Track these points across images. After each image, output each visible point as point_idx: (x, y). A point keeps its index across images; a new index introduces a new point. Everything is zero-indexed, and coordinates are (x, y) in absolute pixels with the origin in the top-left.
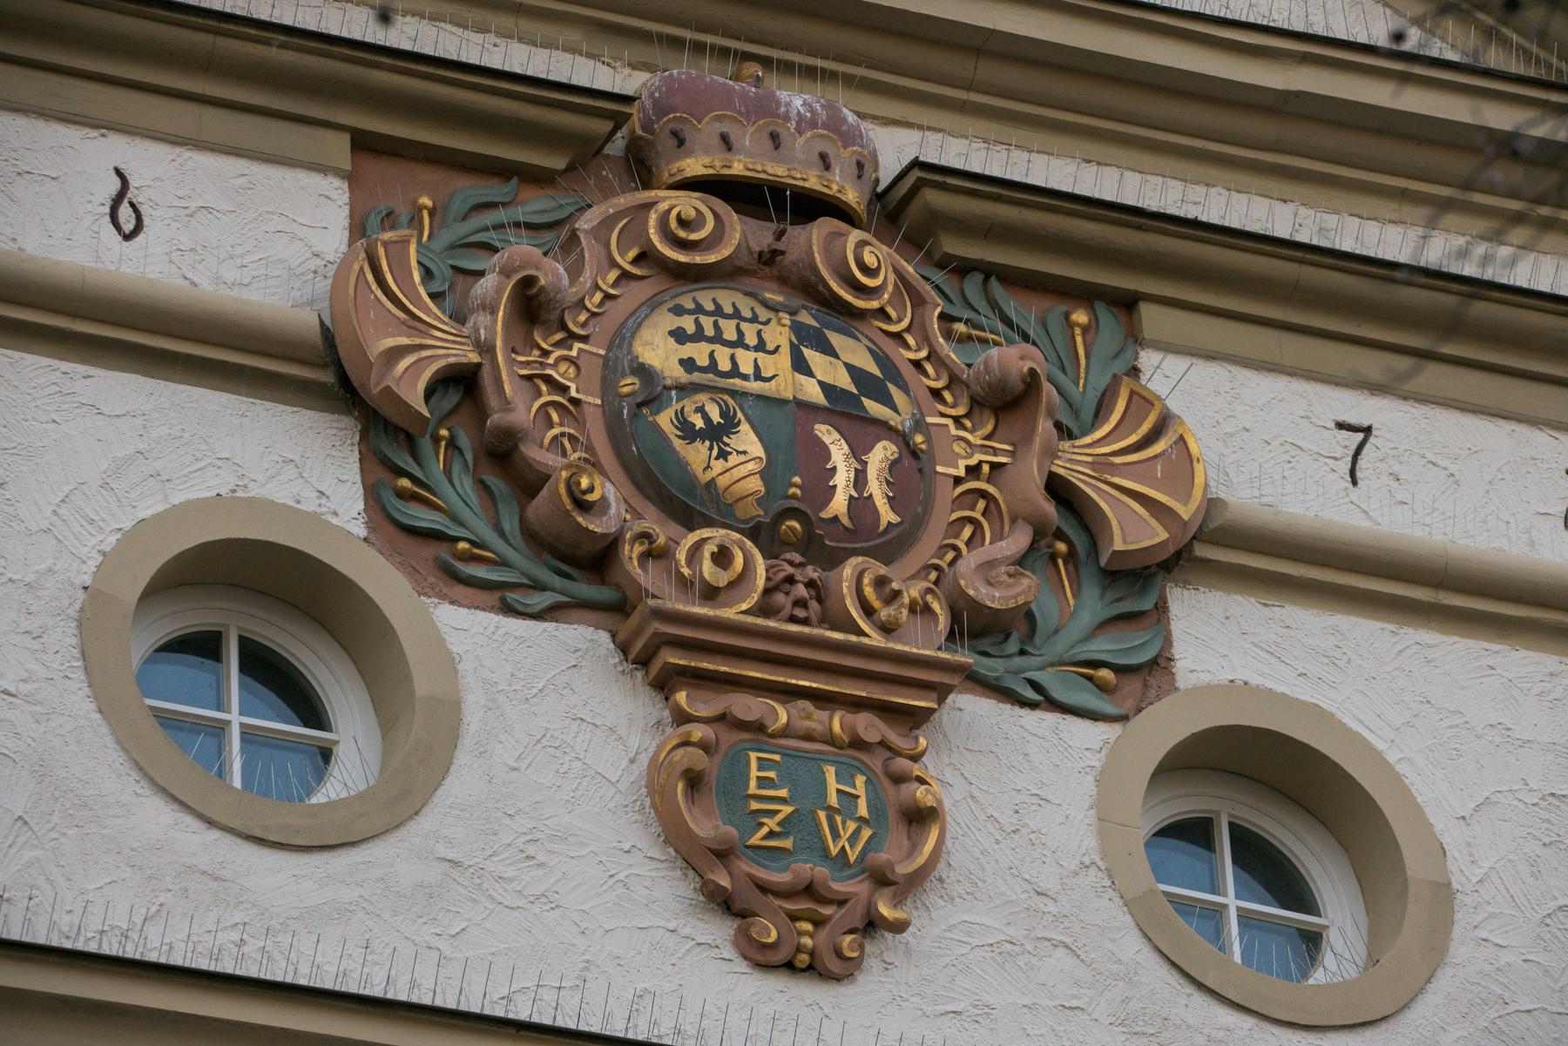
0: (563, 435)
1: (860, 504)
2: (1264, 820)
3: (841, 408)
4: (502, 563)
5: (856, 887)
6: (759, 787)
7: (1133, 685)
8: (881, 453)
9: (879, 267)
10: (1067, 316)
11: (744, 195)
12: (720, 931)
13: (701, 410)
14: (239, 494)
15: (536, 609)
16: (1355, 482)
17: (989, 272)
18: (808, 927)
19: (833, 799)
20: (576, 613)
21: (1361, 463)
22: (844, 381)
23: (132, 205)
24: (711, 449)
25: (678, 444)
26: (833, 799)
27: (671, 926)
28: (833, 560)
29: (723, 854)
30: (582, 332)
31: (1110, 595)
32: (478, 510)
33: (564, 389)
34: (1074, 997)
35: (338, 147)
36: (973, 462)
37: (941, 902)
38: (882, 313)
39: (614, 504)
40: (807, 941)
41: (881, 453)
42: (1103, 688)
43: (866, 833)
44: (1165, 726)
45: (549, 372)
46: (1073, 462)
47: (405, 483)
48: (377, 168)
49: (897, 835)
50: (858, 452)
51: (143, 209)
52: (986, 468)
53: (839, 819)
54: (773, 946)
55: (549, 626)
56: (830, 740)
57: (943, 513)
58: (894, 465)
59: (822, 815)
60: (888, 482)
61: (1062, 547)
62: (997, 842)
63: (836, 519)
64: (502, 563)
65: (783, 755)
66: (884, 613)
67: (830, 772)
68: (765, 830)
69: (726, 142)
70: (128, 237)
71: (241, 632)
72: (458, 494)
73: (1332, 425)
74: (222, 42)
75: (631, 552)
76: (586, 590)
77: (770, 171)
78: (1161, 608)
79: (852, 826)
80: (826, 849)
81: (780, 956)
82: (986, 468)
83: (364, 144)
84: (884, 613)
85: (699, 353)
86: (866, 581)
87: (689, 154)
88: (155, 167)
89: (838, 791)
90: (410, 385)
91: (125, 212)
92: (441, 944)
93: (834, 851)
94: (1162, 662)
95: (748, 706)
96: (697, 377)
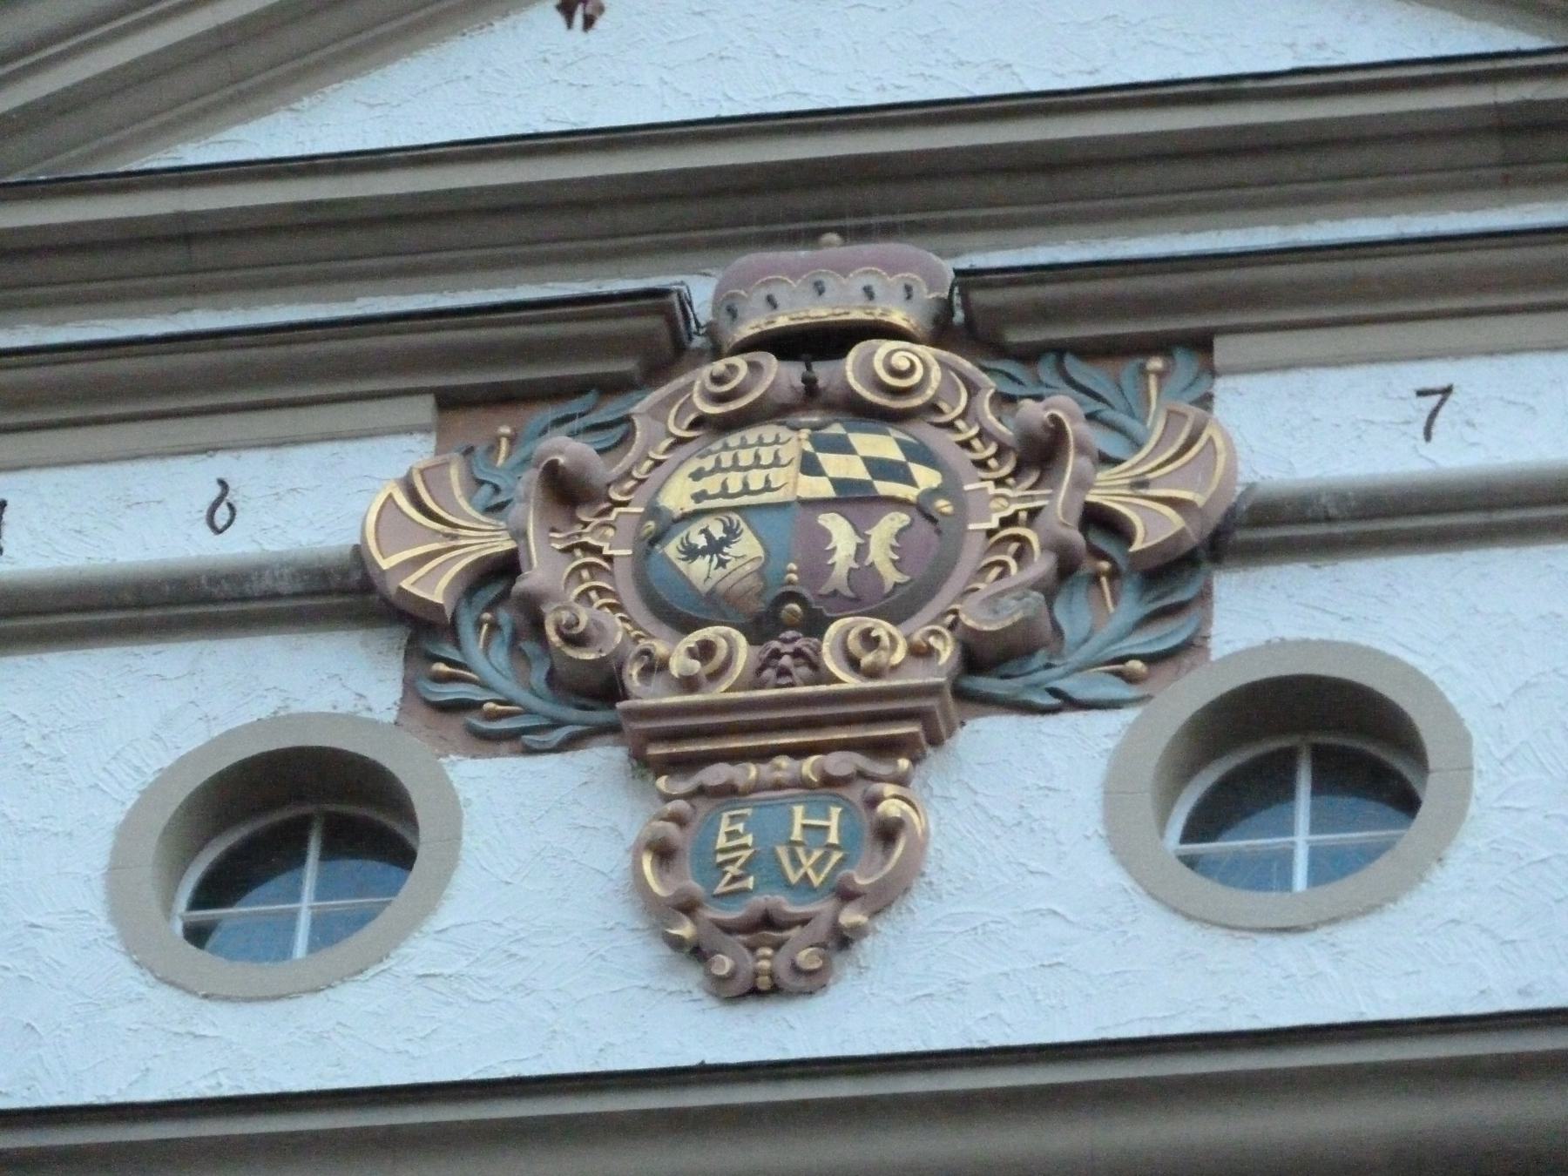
0: (591, 589)
1: (863, 571)
4: (528, 712)
5: (822, 907)
8: (891, 523)
9: (913, 365)
11: (786, 344)
12: (693, 976)
15: (554, 743)
16: (1428, 435)
18: (769, 952)
19: (797, 834)
21: (1439, 420)
22: (859, 472)
25: (681, 565)
26: (797, 834)
28: (815, 625)
29: (688, 907)
31: (1152, 594)
34: (1057, 955)
35: (424, 409)
42: (1131, 679)
43: (836, 856)
44: (1187, 695)
45: (585, 539)
46: (1108, 490)
47: (442, 667)
49: (869, 848)
52: (1023, 515)
54: (732, 975)
55: (568, 755)
57: (972, 554)
59: (783, 853)
61: (1105, 565)
63: (835, 593)
66: (867, 659)
68: (728, 876)
69: (771, 301)
70: (219, 532)
71: (288, 834)
72: (488, 662)
74: (298, 349)
75: (633, 672)
76: (600, 716)
78: (1205, 596)
83: (448, 402)
84: (867, 659)
87: (743, 321)
88: (249, 471)
90: (435, 587)
92: (410, 1048)
93: (794, 878)
94: (1197, 642)
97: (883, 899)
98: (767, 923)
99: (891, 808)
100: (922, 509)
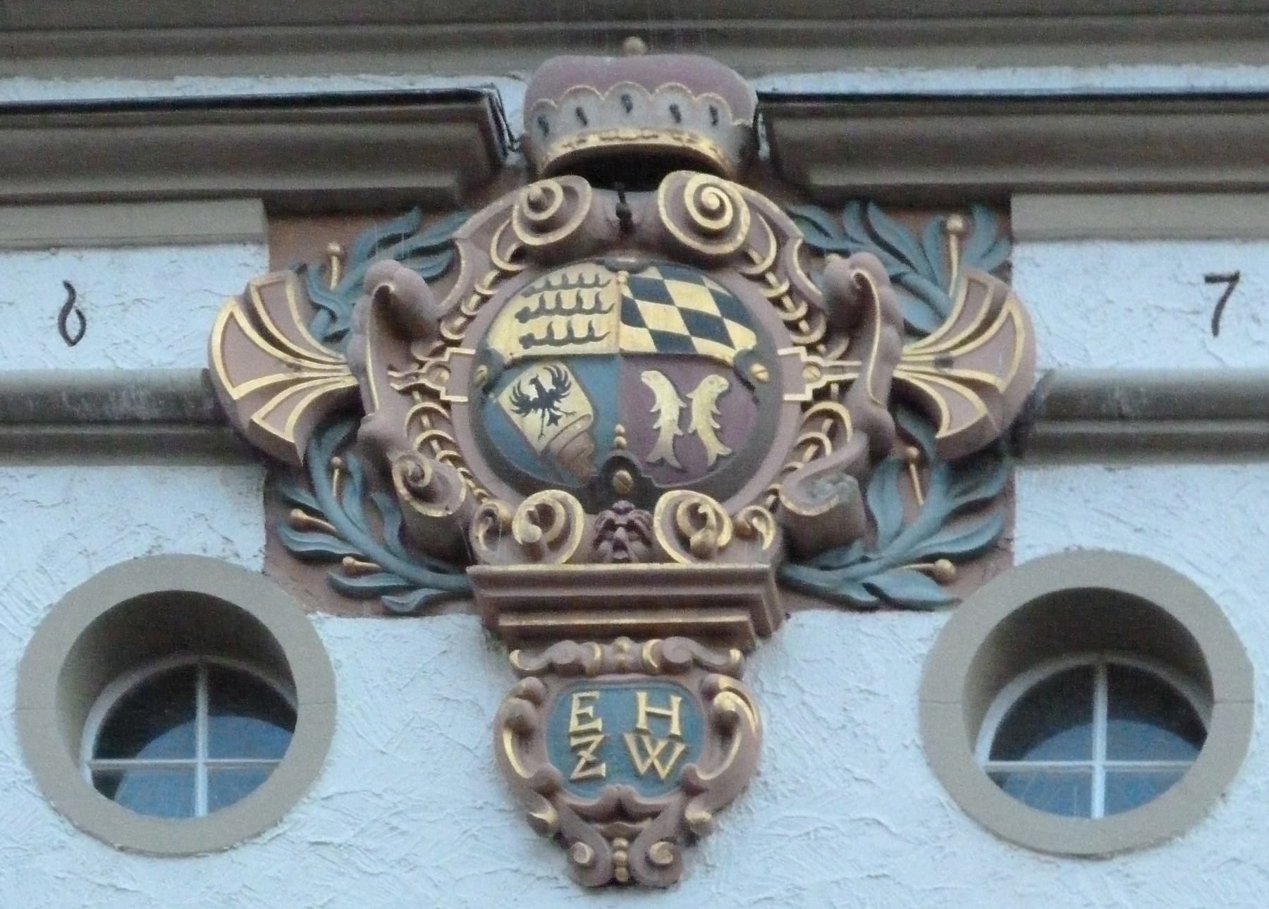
1: (687, 441)
2: (1101, 677)
3: (673, 355)
4: (385, 570)
5: (669, 800)
6: (580, 723)
7: (973, 572)
8: (711, 386)
10: (943, 225)
12: (556, 864)
13: (535, 381)
14: (156, 553)
17: (864, 198)
18: (624, 843)
19: (642, 723)
20: (452, 606)
21: (1226, 312)
22: (678, 326)
23: (79, 313)
24: (543, 416)
25: (515, 418)
26: (642, 723)
27: (513, 866)
28: (645, 496)
30: (456, 337)
31: (959, 488)
32: (362, 525)
33: (434, 395)
34: (882, 866)
35: (252, 216)
36: (821, 384)
37: (764, 803)
38: (743, 256)
39: (462, 488)
40: (621, 855)
41: (711, 386)
42: (941, 580)
43: (679, 748)
44: (994, 601)
46: (914, 366)
47: (299, 514)
48: (293, 232)
49: (708, 742)
50: (682, 390)
51: (87, 315)
52: (835, 388)
53: (646, 740)
56: (644, 668)
57: (789, 430)
58: (720, 399)
59: (630, 739)
60: (714, 415)
61: (913, 452)
62: (824, 740)
63: (662, 462)
64: (385, 570)
65: (602, 690)
66: (696, 538)
67: (642, 696)
68: (583, 762)
70: (73, 343)
71: (175, 684)
72: (342, 508)
73: (1202, 280)
74: (123, 133)
76: (452, 581)
77: (622, 135)
78: (1007, 493)
79: (662, 744)
80: (635, 769)
81: (600, 875)
82: (835, 388)
83: (280, 209)
84: (696, 538)
85: (537, 327)
86: (680, 512)
88: (95, 272)
89: (649, 714)
90: (284, 423)
91: (72, 319)
93: (642, 768)
94: (1001, 544)
95: (565, 652)
96: (535, 350)
97: (725, 796)
98: (620, 813)
99: (727, 701)
100: (737, 372)
